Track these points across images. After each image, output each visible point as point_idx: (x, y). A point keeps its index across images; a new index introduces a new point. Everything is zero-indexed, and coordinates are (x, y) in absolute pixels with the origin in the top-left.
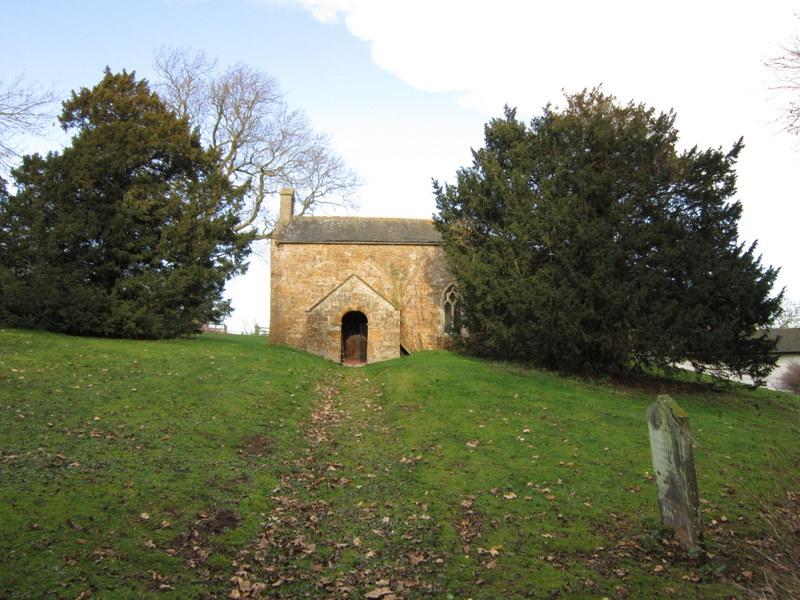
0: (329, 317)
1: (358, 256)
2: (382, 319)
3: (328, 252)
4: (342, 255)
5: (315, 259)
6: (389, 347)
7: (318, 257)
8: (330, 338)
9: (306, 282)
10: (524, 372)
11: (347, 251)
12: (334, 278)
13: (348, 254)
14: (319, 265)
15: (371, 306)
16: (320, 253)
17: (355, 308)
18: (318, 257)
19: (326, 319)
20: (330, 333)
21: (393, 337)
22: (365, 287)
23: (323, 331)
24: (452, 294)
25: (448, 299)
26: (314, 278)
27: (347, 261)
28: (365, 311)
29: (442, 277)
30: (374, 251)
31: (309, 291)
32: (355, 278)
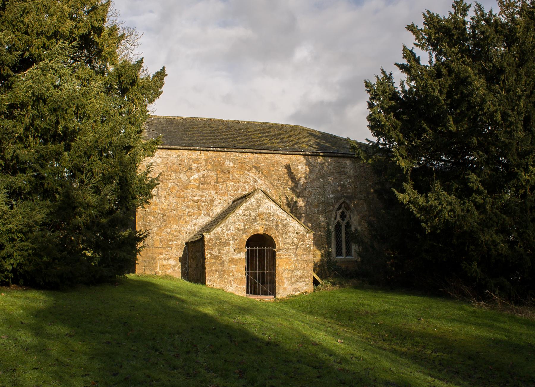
0: (232, 242)
1: (242, 167)
2: (293, 243)
3: (207, 161)
4: (222, 165)
5: (190, 169)
6: (301, 277)
7: (195, 166)
8: (233, 267)
9: (180, 197)
10: (376, 294)
11: (230, 159)
12: (213, 193)
13: (229, 164)
14: (196, 176)
15: (280, 229)
16: (196, 161)
17: (261, 232)
18: (195, 166)
19: (229, 245)
20: (232, 261)
21: (305, 265)
22: (273, 205)
23: (226, 258)
24: (343, 212)
25: (338, 218)
26: (190, 191)
27: (229, 172)
28: (272, 233)
29: (333, 193)
30: (258, 161)
31: (184, 208)
32: (261, 195)
